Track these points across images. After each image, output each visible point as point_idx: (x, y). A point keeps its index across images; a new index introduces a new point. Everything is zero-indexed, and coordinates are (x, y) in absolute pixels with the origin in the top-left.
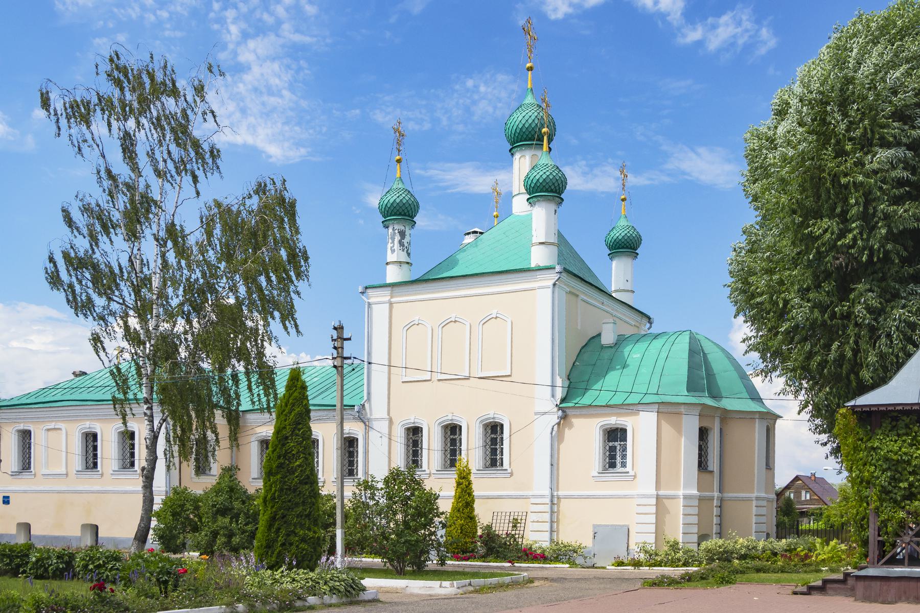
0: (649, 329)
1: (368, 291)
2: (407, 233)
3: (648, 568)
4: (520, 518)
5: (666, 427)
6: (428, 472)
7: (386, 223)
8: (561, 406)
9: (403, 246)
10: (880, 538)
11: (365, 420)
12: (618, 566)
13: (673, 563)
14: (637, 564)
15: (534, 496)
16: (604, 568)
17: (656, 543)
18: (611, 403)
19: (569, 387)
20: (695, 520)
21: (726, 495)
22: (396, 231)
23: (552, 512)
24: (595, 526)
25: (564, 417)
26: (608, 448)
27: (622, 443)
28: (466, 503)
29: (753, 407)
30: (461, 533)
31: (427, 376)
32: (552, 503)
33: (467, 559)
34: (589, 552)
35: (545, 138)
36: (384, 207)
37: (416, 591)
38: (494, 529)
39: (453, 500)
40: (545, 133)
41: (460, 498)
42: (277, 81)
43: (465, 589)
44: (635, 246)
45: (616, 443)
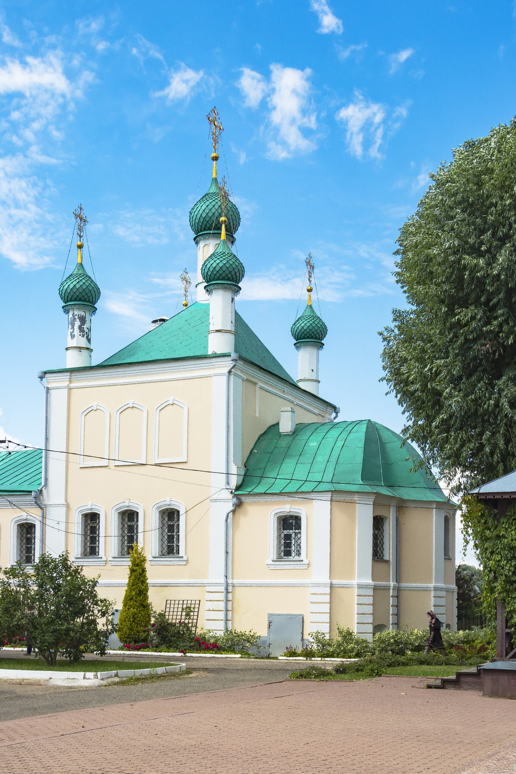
0: (335, 418)
1: (47, 375)
2: (88, 319)
3: (320, 659)
4: (193, 606)
5: (340, 517)
6: (104, 559)
7: (67, 308)
8: (236, 493)
9: (84, 331)
10: (508, 630)
11: (43, 506)
12: (290, 656)
13: (345, 653)
14: (309, 654)
15: (209, 584)
16: (276, 658)
17: (330, 632)
18: (286, 490)
19: (245, 475)
20: (370, 609)
21: (403, 585)
22: (76, 317)
23: (227, 600)
24: (270, 615)
25: (239, 505)
26: (283, 536)
27: (297, 531)
28: (140, 591)
29: (430, 496)
30: (133, 621)
31: (105, 463)
32: (227, 592)
33: (138, 649)
34: (264, 642)
35: (223, 226)
36: (64, 292)
37: (60, 683)
38: (167, 617)
39: (126, 588)
40: (222, 221)
41: (133, 585)
42: (24, 196)
43: (110, 680)
44: (321, 336)
45: (291, 531)
